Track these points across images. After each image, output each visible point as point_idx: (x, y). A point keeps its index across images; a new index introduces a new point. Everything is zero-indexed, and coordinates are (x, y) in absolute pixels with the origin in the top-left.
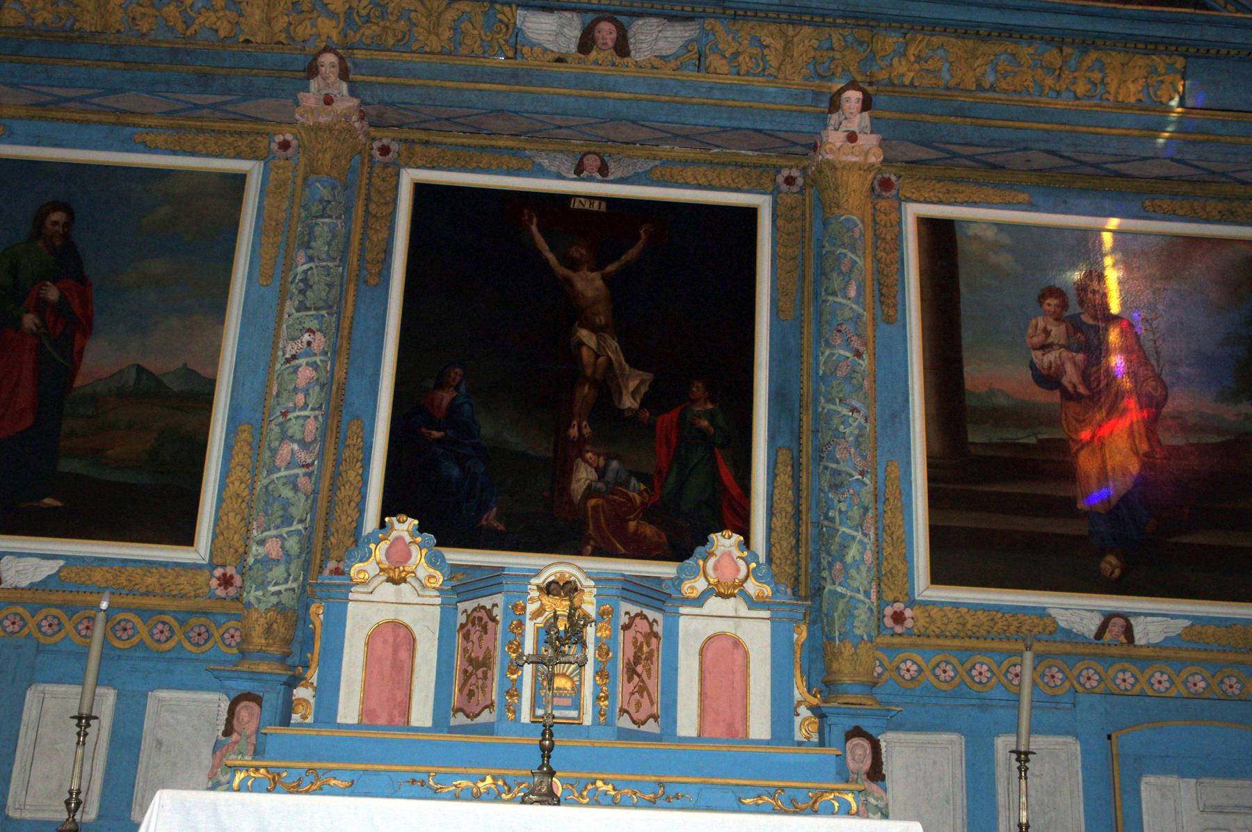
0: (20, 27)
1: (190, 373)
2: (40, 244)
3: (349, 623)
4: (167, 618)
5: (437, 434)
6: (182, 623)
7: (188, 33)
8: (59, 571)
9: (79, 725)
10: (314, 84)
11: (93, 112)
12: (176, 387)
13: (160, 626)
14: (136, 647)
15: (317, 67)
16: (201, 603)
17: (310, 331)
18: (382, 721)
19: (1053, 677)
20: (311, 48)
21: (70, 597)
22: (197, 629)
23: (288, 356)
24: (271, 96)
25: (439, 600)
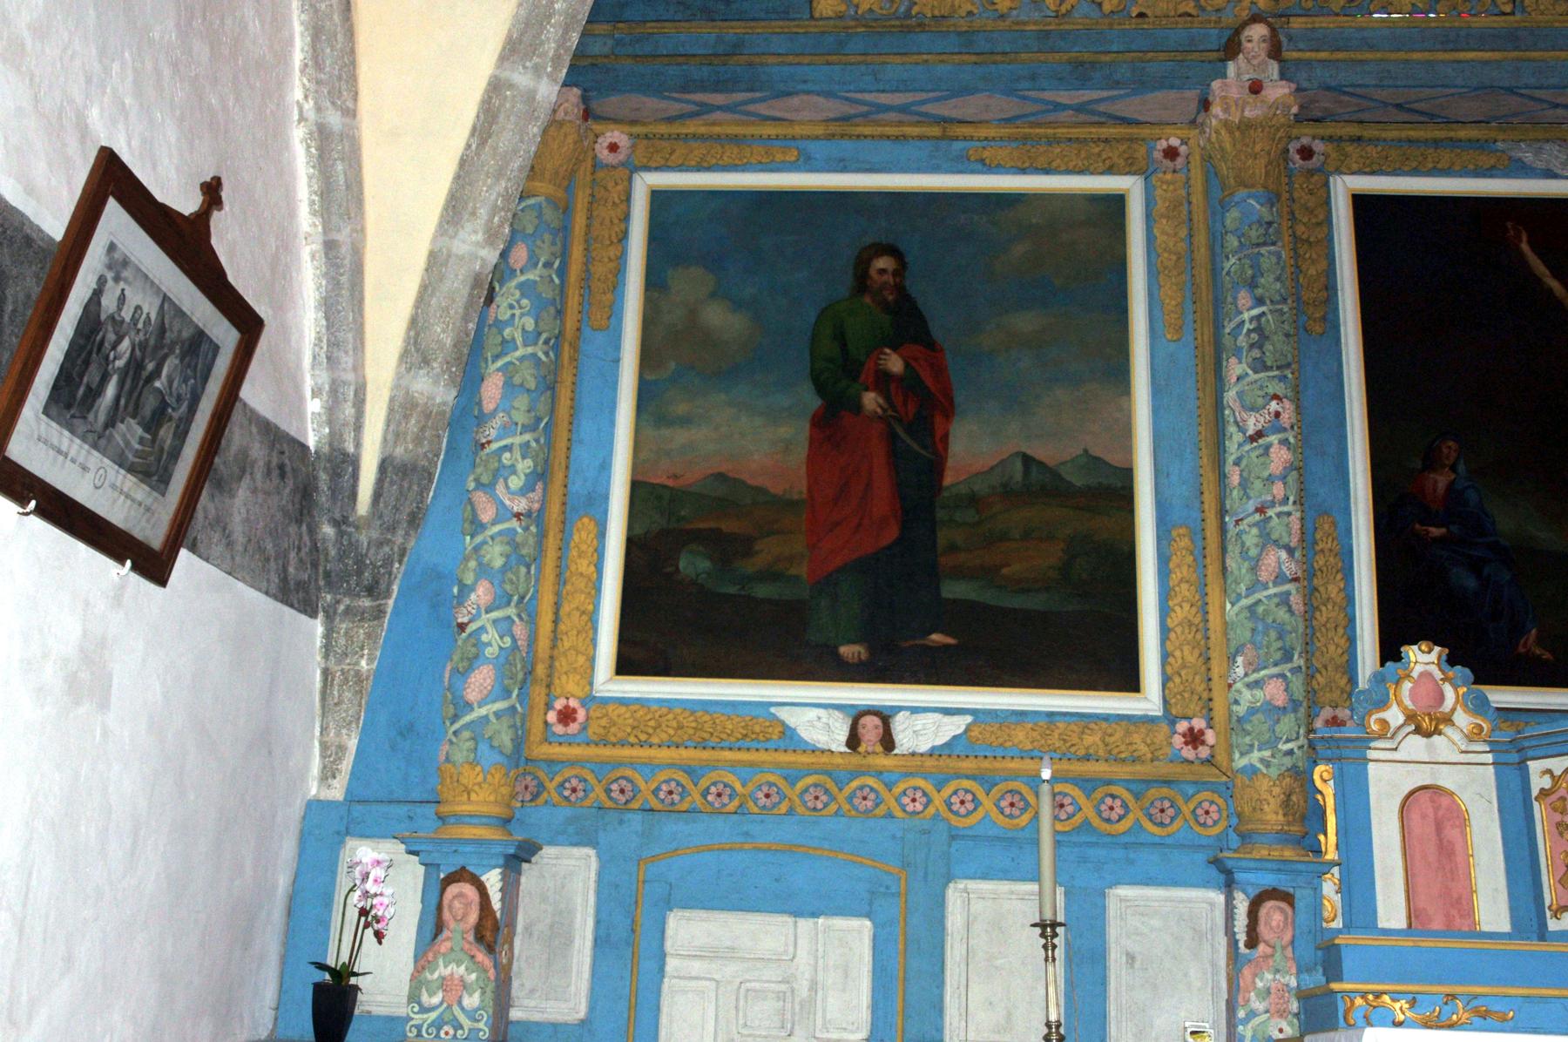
0: (840, 17)
1: (1093, 462)
2: (867, 300)
3: (1373, 791)
4: (1114, 789)
5: (1436, 532)
6: (1137, 796)
7: (1063, 9)
8: (966, 731)
9: (1043, 935)
10: (1231, 67)
11: (911, 124)
12: (1078, 481)
13: (1109, 801)
14: (1078, 829)
15: (1240, 44)
16: (1162, 769)
17: (1275, 397)
18: (1437, 925)
19: (719, 795)
20: (1229, 19)
21: (986, 764)
22: (1158, 804)
23: (1250, 432)
24: (1172, 87)
25: (1489, 758)
